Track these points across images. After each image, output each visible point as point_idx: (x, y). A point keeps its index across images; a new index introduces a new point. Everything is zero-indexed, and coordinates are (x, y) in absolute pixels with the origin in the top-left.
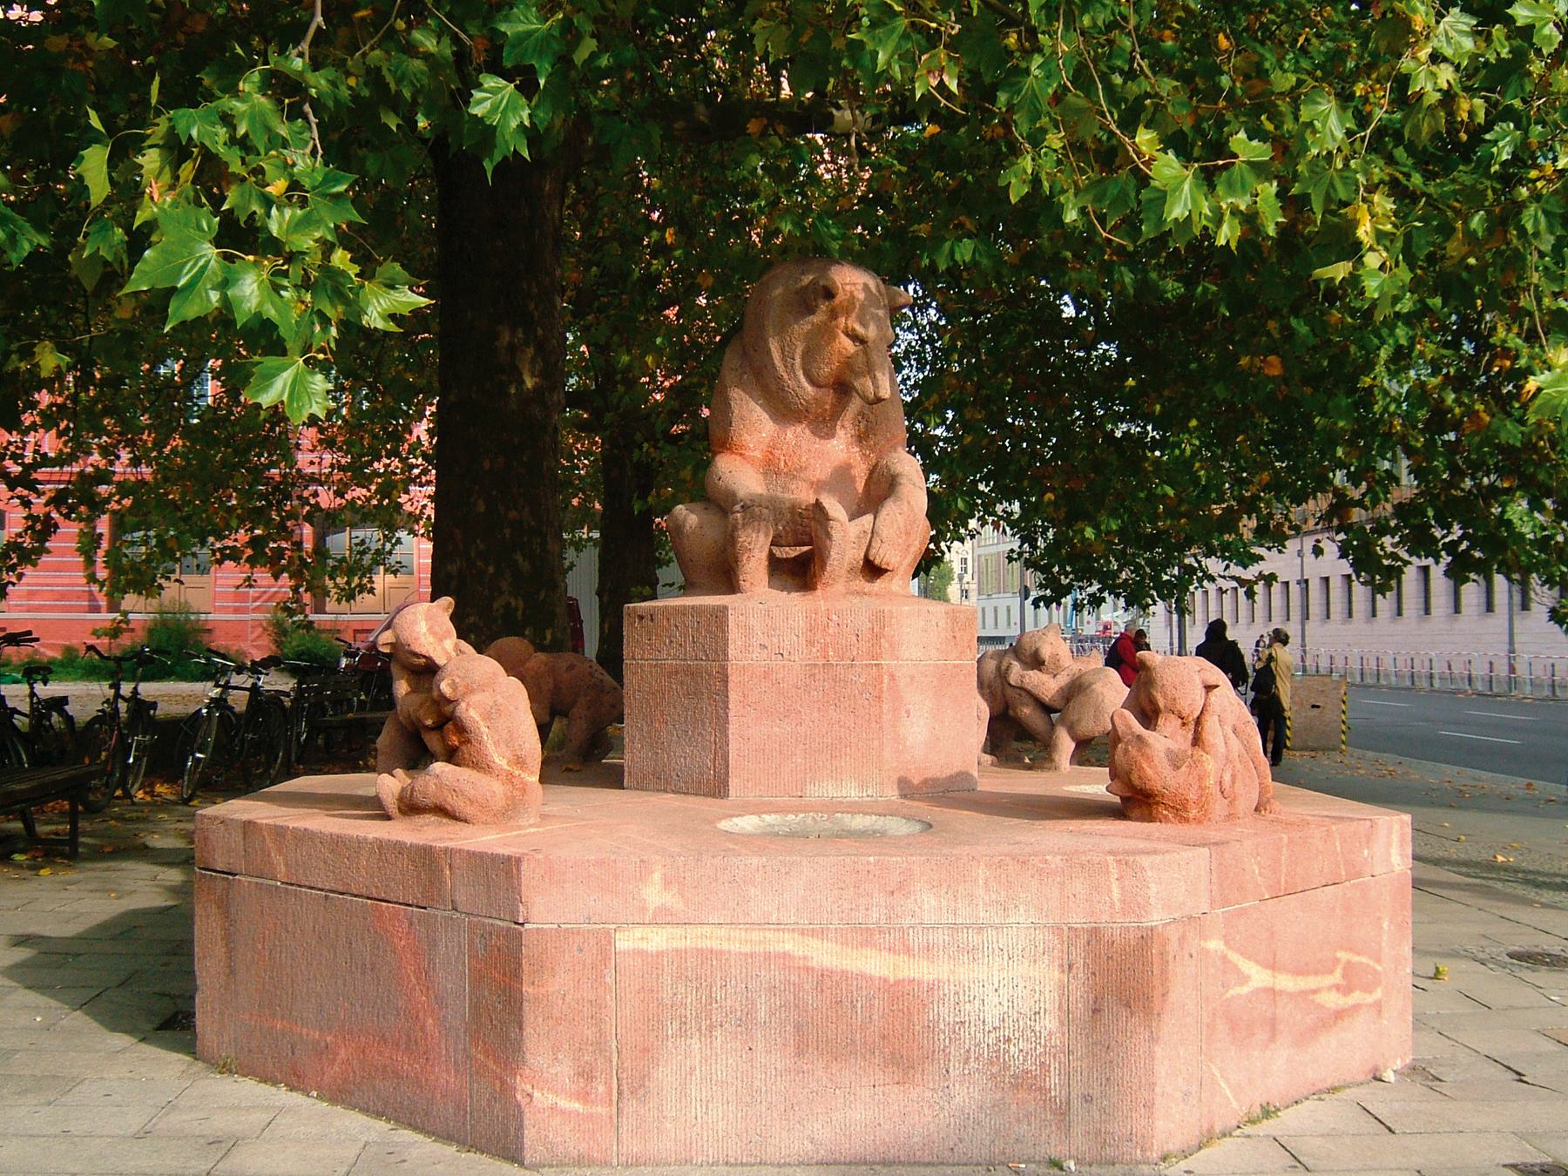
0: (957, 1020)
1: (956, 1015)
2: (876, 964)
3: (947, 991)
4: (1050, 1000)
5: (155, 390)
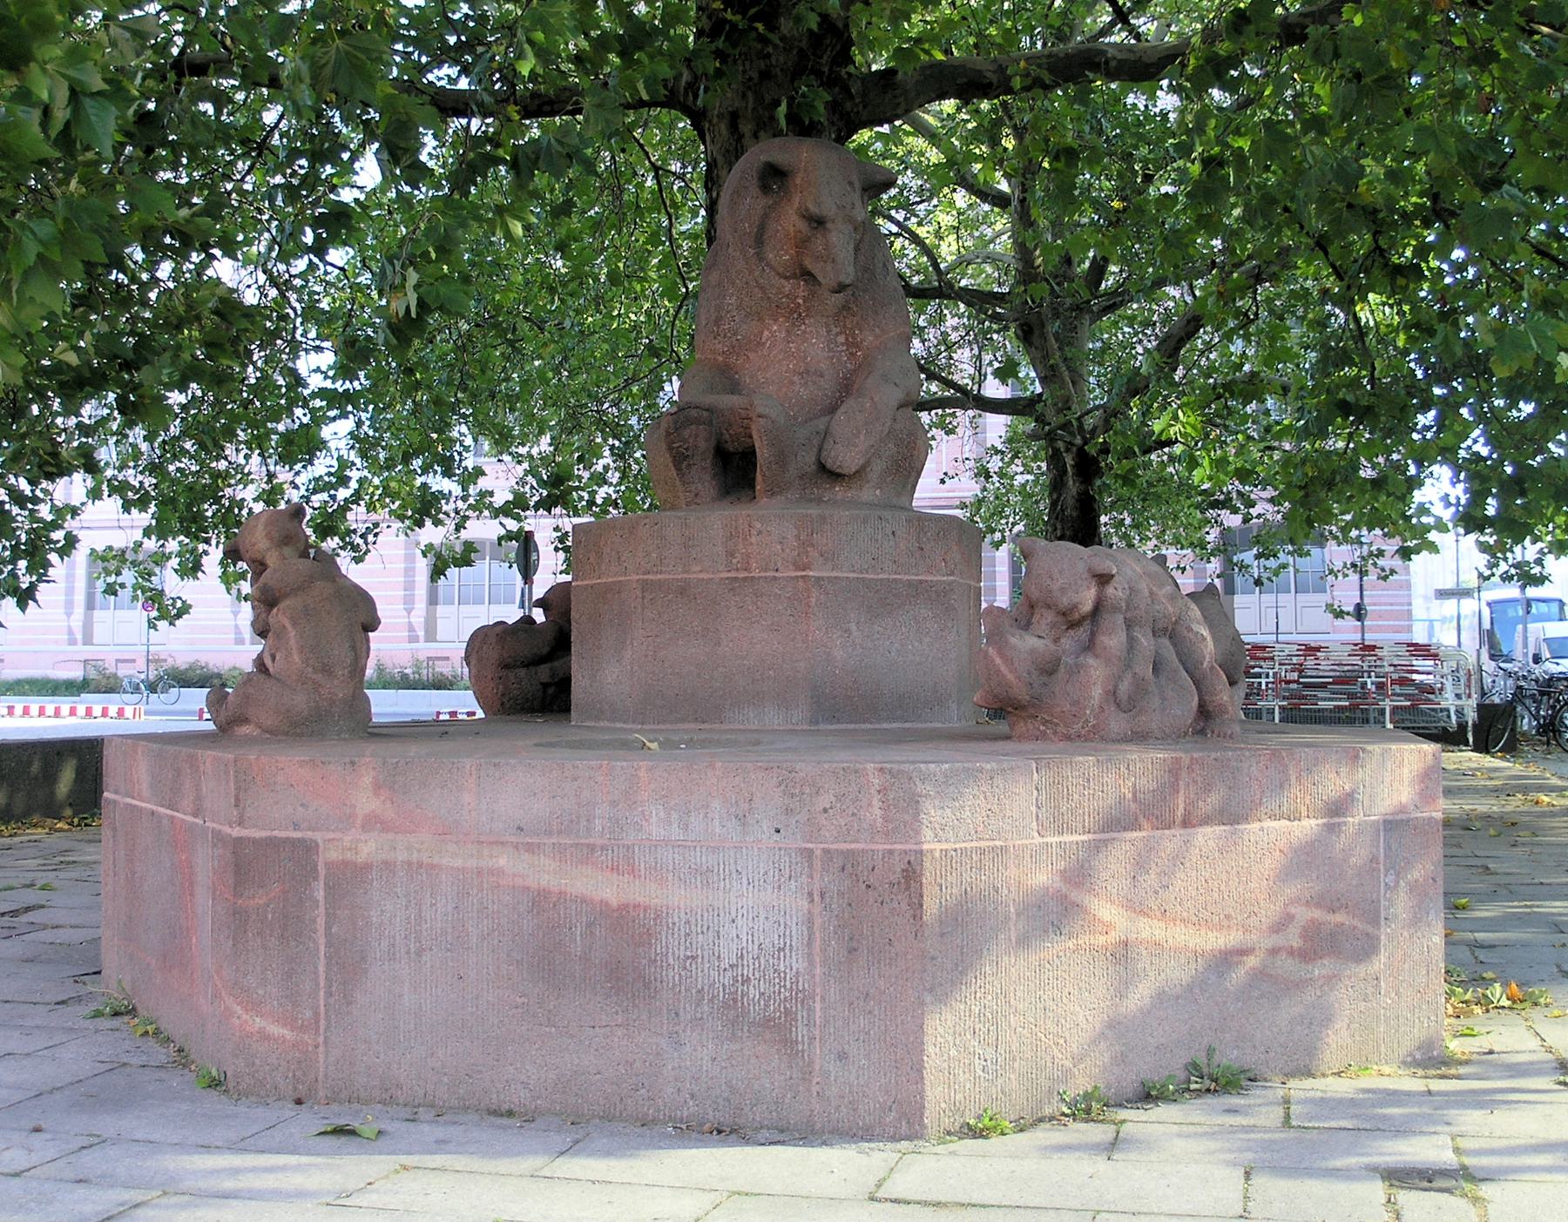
0: (689, 954)
1: (686, 948)
2: (606, 888)
3: (676, 920)
4: (797, 933)
5: (513, 347)
